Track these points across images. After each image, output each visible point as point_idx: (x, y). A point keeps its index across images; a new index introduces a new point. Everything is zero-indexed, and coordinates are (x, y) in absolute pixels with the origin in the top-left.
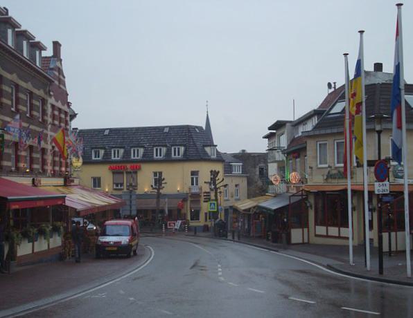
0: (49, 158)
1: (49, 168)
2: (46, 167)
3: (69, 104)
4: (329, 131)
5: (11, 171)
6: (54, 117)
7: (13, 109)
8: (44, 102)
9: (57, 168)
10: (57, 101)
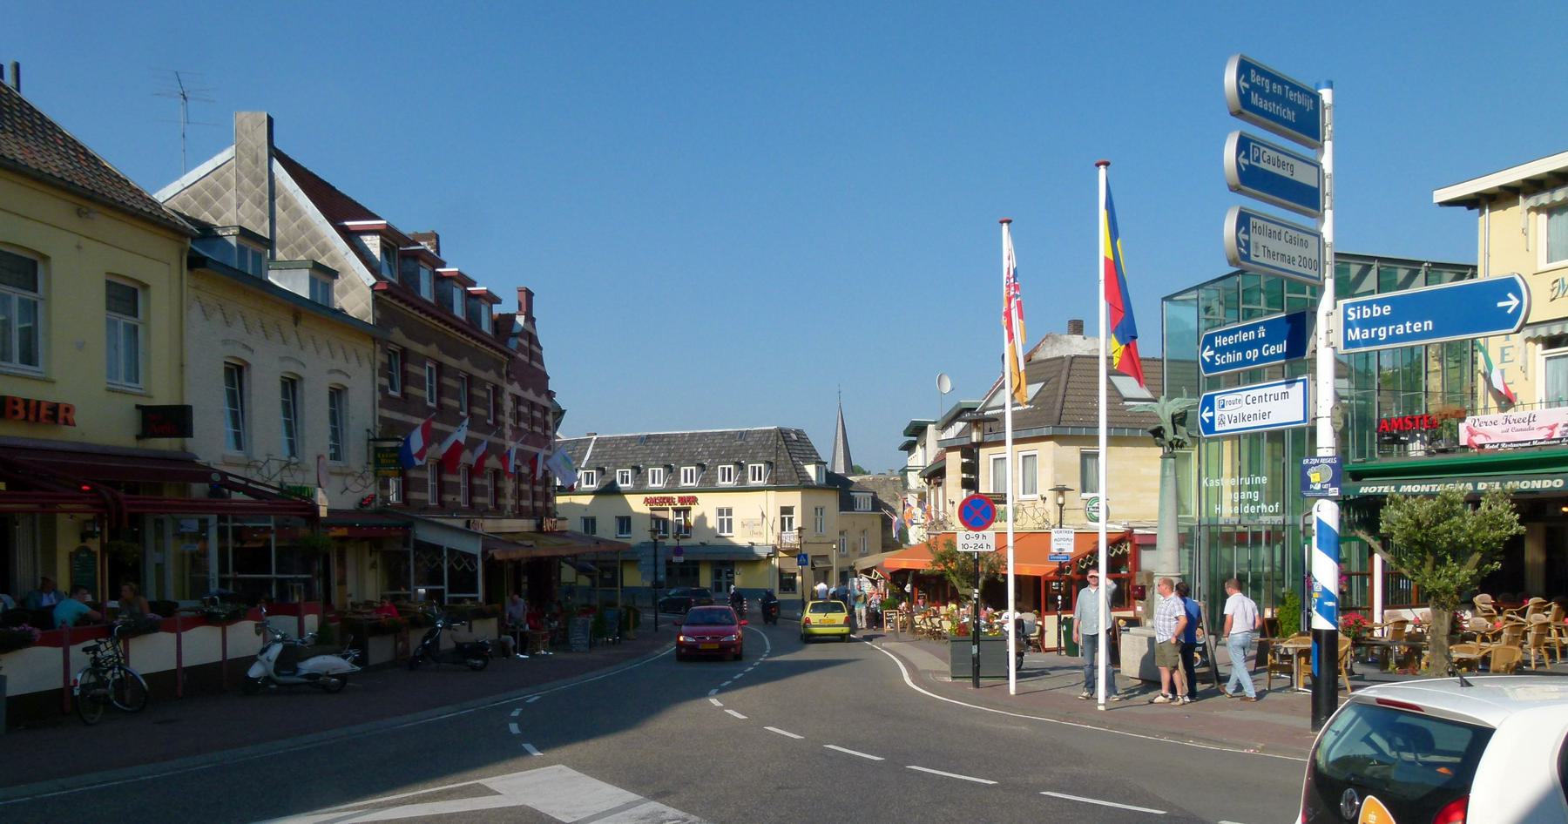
0: (509, 486)
1: (509, 502)
2: (501, 501)
3: (550, 395)
4: (1034, 433)
5: (487, 511)
6: (518, 417)
7: (490, 422)
8: (497, 391)
9: (525, 503)
10: (525, 388)
